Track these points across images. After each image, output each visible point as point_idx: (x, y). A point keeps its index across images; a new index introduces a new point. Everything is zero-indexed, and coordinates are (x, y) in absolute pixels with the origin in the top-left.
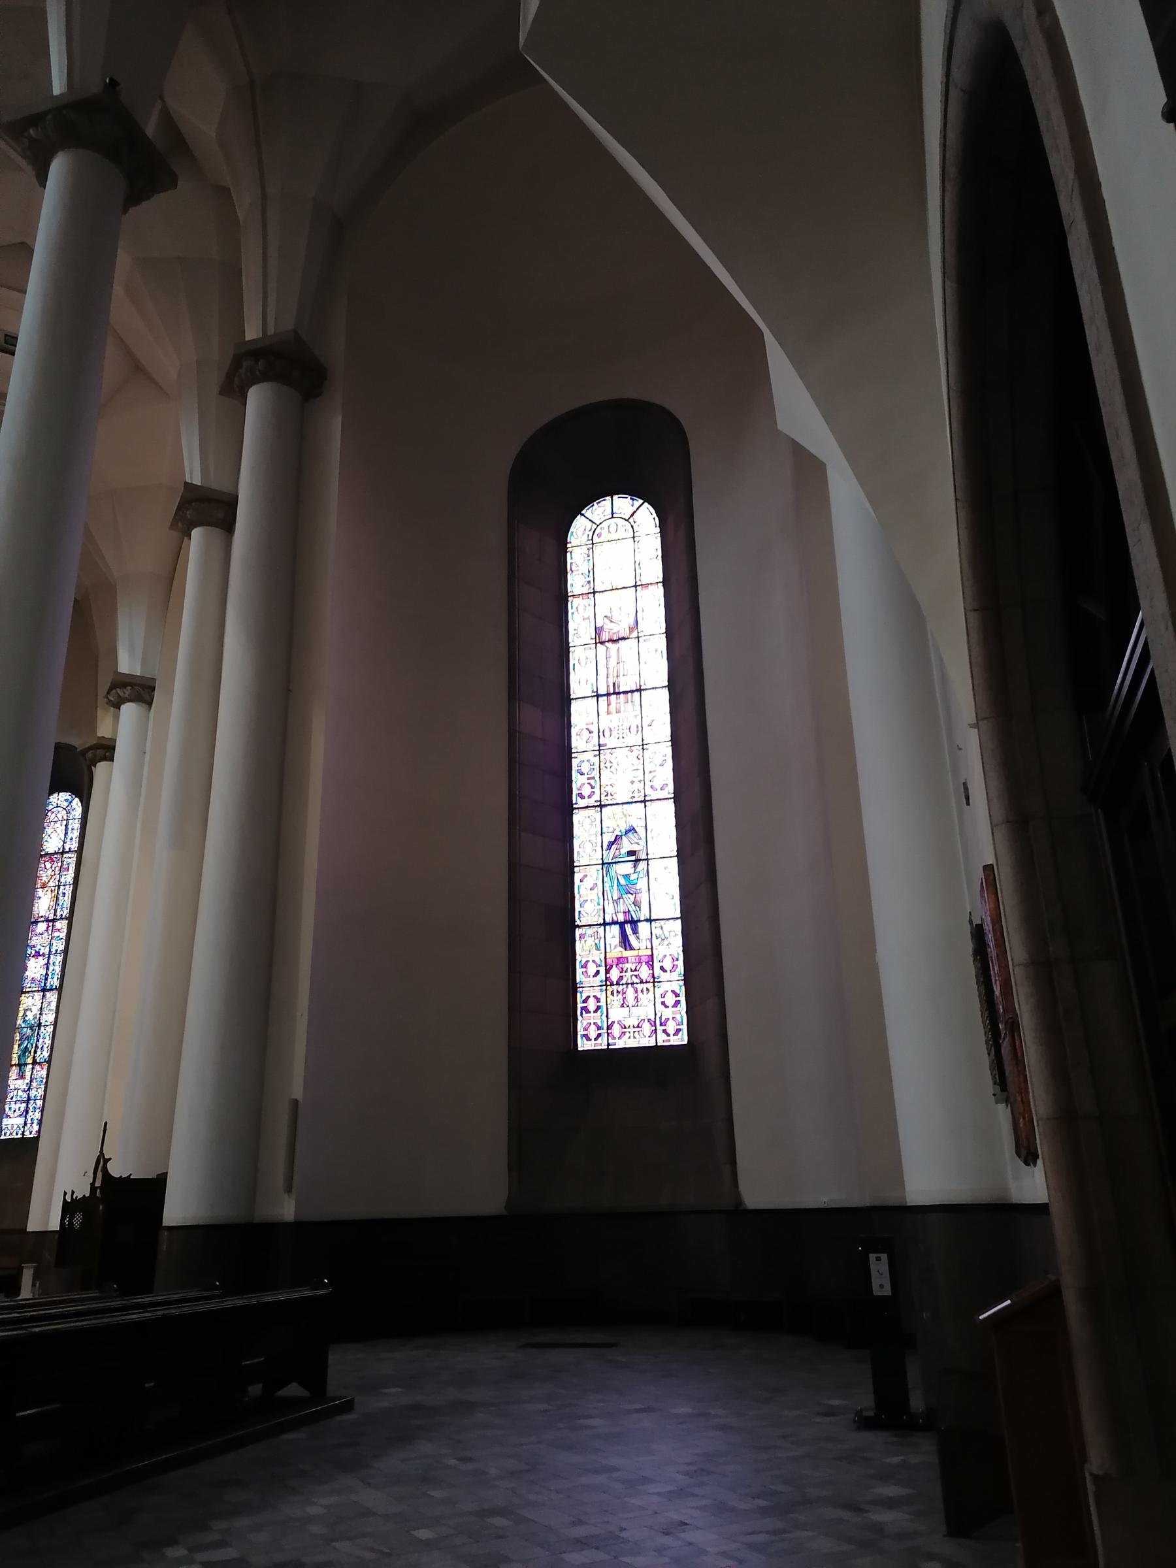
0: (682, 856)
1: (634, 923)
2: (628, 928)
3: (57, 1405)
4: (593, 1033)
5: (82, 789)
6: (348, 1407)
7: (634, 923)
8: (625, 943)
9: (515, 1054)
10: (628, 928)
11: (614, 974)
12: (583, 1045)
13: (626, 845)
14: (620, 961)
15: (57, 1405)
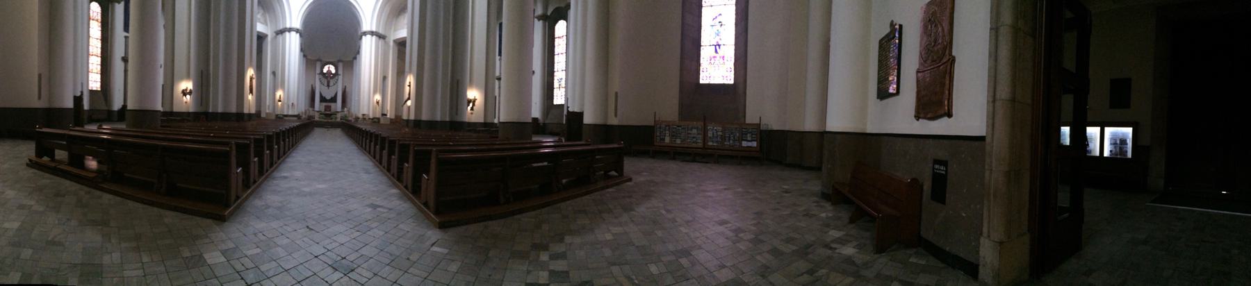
0: (698, 46)
1: (719, 45)
2: (717, 47)
3: (535, 165)
4: (705, 78)
5: (565, 18)
6: (630, 180)
7: (719, 45)
8: (716, 51)
9: (681, 83)
10: (717, 47)
11: (712, 62)
12: (701, 82)
13: (719, 19)
14: (714, 57)
15: (535, 165)
